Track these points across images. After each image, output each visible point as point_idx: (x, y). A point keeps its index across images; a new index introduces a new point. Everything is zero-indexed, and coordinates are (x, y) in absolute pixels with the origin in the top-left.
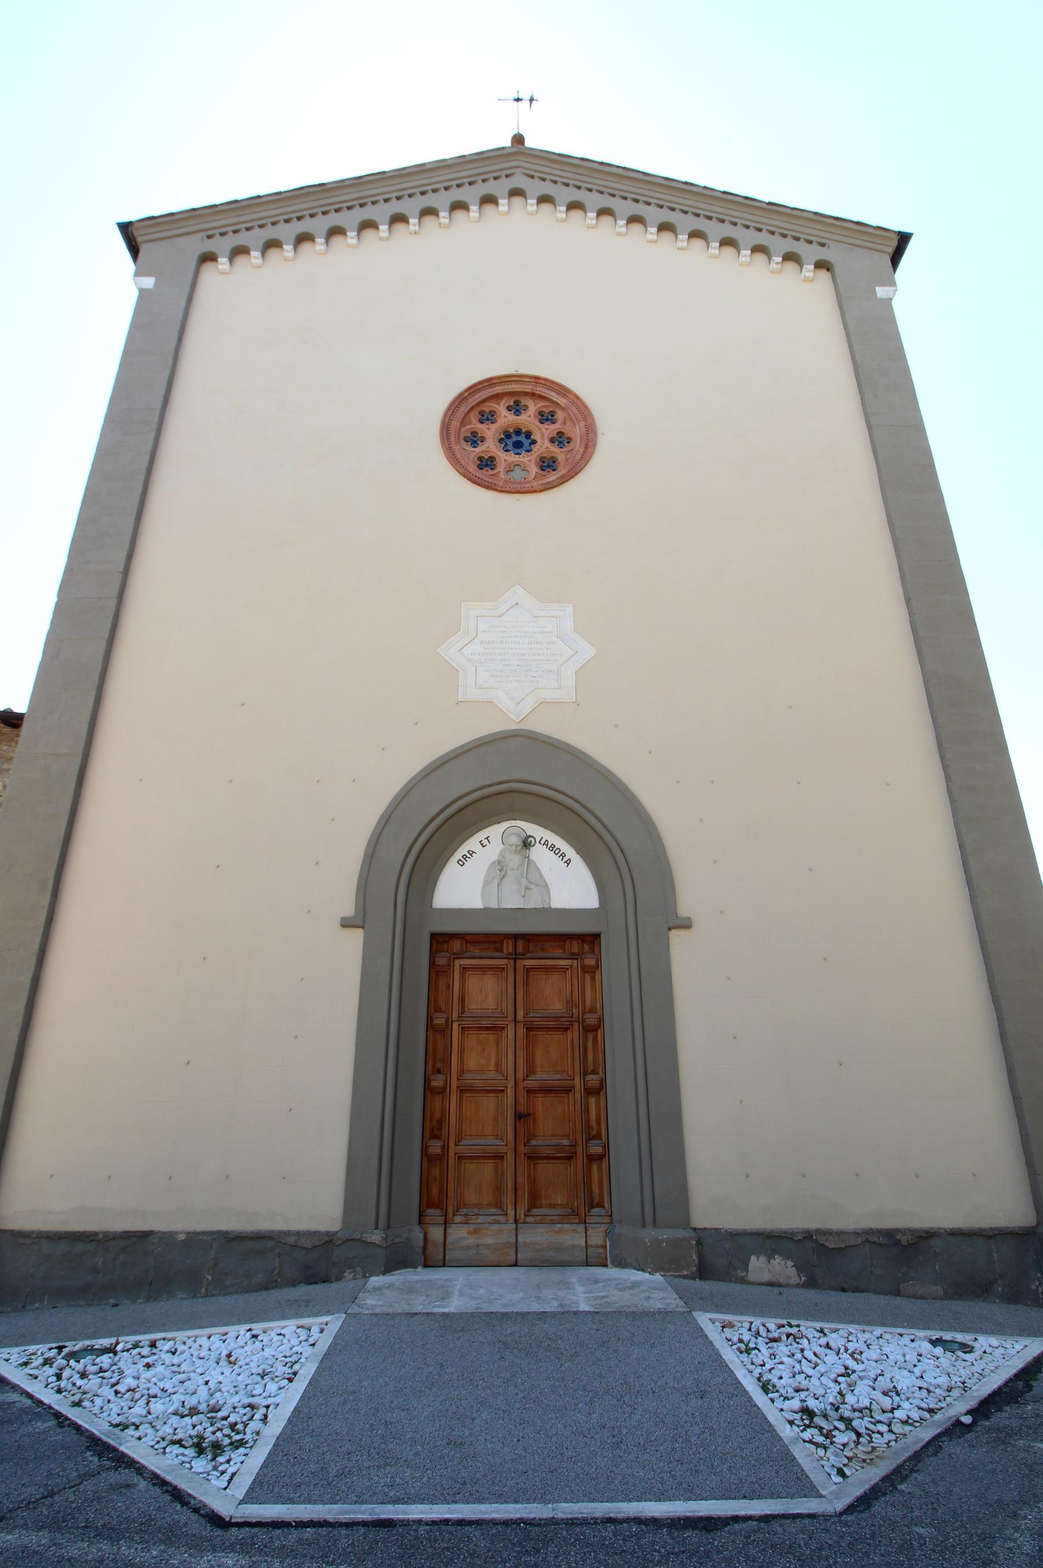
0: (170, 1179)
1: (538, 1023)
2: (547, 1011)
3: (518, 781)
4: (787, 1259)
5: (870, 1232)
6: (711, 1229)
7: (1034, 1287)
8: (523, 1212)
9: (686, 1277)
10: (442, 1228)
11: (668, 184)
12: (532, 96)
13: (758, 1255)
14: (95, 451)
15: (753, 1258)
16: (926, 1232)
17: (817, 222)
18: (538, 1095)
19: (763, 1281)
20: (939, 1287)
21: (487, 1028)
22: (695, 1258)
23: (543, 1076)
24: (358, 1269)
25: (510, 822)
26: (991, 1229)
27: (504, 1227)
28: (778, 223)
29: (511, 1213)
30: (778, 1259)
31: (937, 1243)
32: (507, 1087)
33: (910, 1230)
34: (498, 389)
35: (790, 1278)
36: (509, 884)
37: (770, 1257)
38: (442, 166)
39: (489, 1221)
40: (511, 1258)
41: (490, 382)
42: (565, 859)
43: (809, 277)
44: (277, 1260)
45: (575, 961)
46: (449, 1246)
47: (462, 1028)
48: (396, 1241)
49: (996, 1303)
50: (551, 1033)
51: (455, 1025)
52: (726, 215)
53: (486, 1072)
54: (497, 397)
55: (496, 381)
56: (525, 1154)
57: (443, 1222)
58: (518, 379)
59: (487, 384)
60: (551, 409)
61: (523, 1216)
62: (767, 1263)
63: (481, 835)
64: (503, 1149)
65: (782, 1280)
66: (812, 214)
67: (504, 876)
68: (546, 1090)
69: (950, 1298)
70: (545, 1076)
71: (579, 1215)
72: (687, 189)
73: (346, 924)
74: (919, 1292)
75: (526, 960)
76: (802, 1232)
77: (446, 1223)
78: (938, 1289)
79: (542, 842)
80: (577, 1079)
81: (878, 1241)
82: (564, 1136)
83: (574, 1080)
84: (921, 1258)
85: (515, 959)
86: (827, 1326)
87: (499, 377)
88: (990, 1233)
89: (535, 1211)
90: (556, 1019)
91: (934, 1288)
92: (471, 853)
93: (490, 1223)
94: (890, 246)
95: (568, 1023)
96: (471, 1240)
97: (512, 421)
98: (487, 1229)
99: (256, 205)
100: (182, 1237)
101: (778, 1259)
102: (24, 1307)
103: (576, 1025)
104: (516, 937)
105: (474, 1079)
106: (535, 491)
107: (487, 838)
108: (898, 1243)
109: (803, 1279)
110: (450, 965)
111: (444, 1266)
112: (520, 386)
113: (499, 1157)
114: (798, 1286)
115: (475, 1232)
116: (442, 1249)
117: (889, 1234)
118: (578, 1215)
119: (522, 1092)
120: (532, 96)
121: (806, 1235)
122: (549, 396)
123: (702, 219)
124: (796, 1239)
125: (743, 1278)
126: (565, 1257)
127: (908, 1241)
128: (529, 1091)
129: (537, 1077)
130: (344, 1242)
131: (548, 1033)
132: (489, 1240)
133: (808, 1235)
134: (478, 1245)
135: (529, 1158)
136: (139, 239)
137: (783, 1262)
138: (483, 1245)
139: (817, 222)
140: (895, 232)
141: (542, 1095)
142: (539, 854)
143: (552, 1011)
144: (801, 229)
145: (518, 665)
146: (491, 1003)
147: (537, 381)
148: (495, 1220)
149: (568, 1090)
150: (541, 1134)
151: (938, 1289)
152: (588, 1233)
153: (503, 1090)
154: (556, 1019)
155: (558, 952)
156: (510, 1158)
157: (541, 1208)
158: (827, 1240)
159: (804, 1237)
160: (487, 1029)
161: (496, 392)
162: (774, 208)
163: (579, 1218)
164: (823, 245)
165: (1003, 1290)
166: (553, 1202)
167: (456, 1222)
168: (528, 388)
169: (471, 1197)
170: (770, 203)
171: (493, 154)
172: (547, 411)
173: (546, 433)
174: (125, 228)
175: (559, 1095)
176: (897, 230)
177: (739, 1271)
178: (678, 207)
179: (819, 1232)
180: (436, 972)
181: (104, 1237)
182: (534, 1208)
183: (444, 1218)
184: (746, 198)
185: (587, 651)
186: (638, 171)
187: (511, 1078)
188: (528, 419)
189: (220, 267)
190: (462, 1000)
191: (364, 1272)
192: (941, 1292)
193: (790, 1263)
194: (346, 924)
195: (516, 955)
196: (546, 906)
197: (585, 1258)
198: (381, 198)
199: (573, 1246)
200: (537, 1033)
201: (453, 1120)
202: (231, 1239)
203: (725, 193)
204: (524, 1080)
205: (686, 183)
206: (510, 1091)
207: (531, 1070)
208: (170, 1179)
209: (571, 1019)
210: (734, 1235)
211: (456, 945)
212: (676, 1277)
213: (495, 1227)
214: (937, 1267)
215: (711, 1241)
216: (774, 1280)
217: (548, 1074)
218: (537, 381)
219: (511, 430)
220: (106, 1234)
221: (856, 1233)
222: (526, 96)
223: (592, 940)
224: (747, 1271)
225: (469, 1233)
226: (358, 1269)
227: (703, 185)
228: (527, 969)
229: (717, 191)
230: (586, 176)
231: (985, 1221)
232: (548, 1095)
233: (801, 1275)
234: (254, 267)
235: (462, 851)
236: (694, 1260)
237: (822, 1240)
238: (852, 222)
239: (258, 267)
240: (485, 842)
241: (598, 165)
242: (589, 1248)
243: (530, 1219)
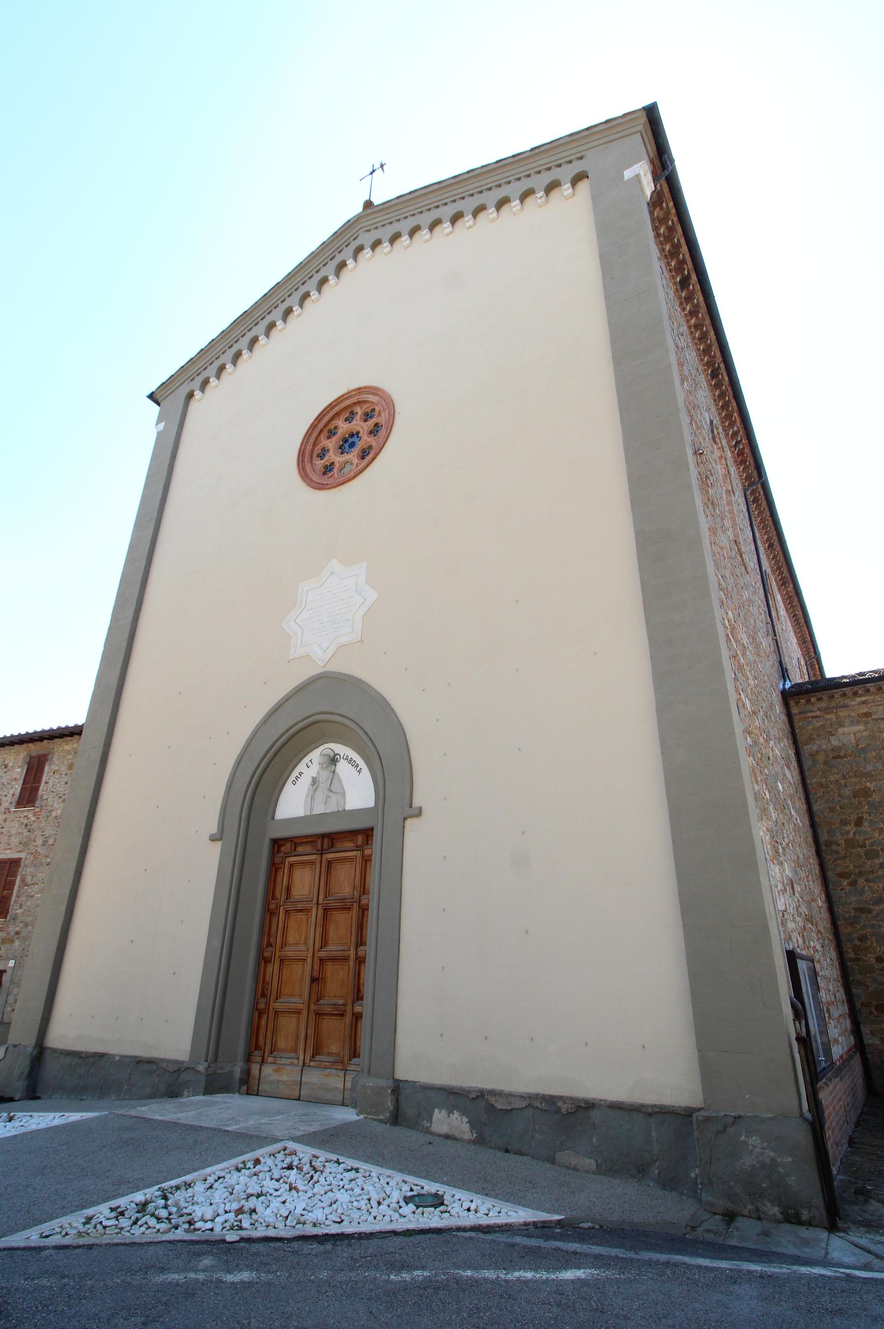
0: (442, 1036)
1: (331, 905)
2: (340, 895)
3: (320, 713)
4: (464, 1114)
5: (536, 1097)
6: (411, 1081)
7: (693, 1175)
8: (309, 1057)
9: (381, 1121)
10: (259, 1066)
11: (457, 181)
12: (381, 163)
13: (441, 1108)
14: (128, 548)
15: (437, 1111)
16: (586, 1101)
17: (573, 141)
18: (328, 963)
19: (442, 1133)
20: (592, 1161)
21: (301, 910)
22: (389, 1105)
23: (333, 948)
24: (191, 1090)
25: (324, 745)
26: (655, 1106)
27: (295, 1068)
28: (543, 161)
29: (301, 1057)
30: (456, 1114)
31: (596, 1115)
32: (307, 957)
33: (571, 1099)
34: (337, 409)
35: (464, 1133)
36: (320, 795)
37: (450, 1112)
38: (313, 256)
39: (287, 1062)
40: (296, 1093)
41: (331, 406)
42: (358, 769)
43: (569, 194)
44: (157, 1079)
45: (359, 852)
46: (262, 1080)
47: (286, 911)
48: (219, 1071)
49: (649, 1186)
50: (341, 912)
51: (282, 908)
52: (437, 202)
53: (298, 945)
54: (337, 415)
55: (335, 404)
56: (314, 1011)
57: (261, 1061)
58: (348, 395)
59: (329, 409)
60: (372, 408)
61: (308, 1060)
62: (447, 1116)
63: (306, 760)
64: (301, 1006)
65: (457, 1134)
66: (567, 137)
67: (316, 789)
68: (333, 959)
69: (604, 1174)
70: (334, 948)
71: (341, 1064)
72: (472, 175)
73: (213, 839)
74: (573, 1163)
75: (328, 855)
76: (476, 1091)
77: (263, 1062)
78: (591, 1163)
79: (345, 758)
80: (352, 950)
81: (540, 1107)
82: (342, 997)
83: (350, 950)
84: (579, 1128)
85: (322, 854)
86: (363, 1167)
87: (336, 400)
88: (650, 1110)
89: (318, 1058)
90: (342, 901)
91: (588, 1161)
92: (301, 774)
93: (288, 1065)
94: (640, 124)
95: (350, 904)
96: (275, 1077)
97: (346, 428)
98: (284, 1069)
99: (214, 345)
100: (117, 1058)
101: (456, 1114)
102: (51, 1096)
103: (355, 905)
104: (323, 836)
105: (289, 951)
106: (349, 480)
107: (311, 761)
108: (558, 1111)
109: (475, 1135)
110: (283, 862)
111: (257, 1095)
112: (348, 401)
113: (298, 1012)
114: (470, 1141)
115: (277, 1071)
116: (257, 1082)
117: (551, 1099)
118: (342, 1063)
119: (317, 961)
120: (381, 163)
121: (479, 1094)
122: (367, 399)
123: (575, 163)
124: (471, 1097)
125: (428, 1128)
126: (329, 1096)
127: (568, 1109)
128: (322, 960)
129: (330, 948)
130: (185, 1070)
131: (340, 912)
132: (285, 1078)
133: (482, 1094)
134: (278, 1081)
135: (316, 1014)
136: (159, 401)
137: (460, 1118)
138: (281, 1081)
139: (573, 141)
140: (640, 110)
141: (331, 963)
142: (343, 767)
143: (343, 894)
144: (567, 153)
145: (328, 622)
146: (306, 891)
147: (360, 391)
148: (292, 1062)
149: (346, 959)
150: (328, 995)
151: (591, 1163)
152: (346, 1078)
153: (305, 959)
154: (342, 901)
155: (350, 845)
156: (305, 1013)
157: (322, 1055)
158: (496, 1100)
159: (477, 1097)
160: (301, 911)
161: (335, 412)
162: (537, 151)
163: (343, 1065)
164: (581, 158)
165: (659, 1173)
166: (331, 1051)
167: (269, 1061)
168: (354, 400)
169: (282, 1043)
170: (532, 150)
171: (343, 229)
172: (369, 411)
173: (366, 428)
174: (151, 397)
175: (342, 963)
176: (640, 107)
177: (425, 1121)
178: (532, 172)
179: (492, 1093)
180: (274, 867)
181: (85, 1055)
182: (319, 1055)
183: (261, 1058)
184: (514, 156)
185: (372, 595)
186: (434, 184)
187: (311, 950)
188: (343, 427)
189: (196, 397)
190: (289, 889)
191: (194, 1092)
192: (593, 1167)
193: (465, 1119)
194: (213, 839)
195: (322, 850)
196: (340, 809)
197: (342, 1098)
198: (279, 302)
199: (336, 1088)
200: (333, 912)
201: (275, 983)
202: (139, 1061)
203: (497, 162)
204: (319, 951)
205: (468, 172)
206: (309, 960)
207: (324, 943)
208: (442, 1036)
209: (352, 900)
210: (427, 1088)
211: (288, 847)
212: (374, 1120)
213: (289, 1068)
214: (594, 1140)
215: (408, 1091)
216: (450, 1133)
217: (336, 946)
218: (360, 391)
219: (347, 436)
220: (87, 1053)
221: (522, 1097)
222: (377, 166)
223: (367, 833)
224: (431, 1123)
225: (275, 1071)
226: (191, 1090)
227: (529, 149)
228: (329, 861)
229: (492, 164)
230: (403, 208)
231: (650, 1098)
232: (335, 963)
233: (473, 1132)
234: (214, 388)
235: (295, 773)
236: (389, 1107)
237: (492, 1100)
238: (601, 124)
239: (216, 387)
240: (310, 764)
241: (409, 195)
242: (346, 1091)
243: (312, 1064)
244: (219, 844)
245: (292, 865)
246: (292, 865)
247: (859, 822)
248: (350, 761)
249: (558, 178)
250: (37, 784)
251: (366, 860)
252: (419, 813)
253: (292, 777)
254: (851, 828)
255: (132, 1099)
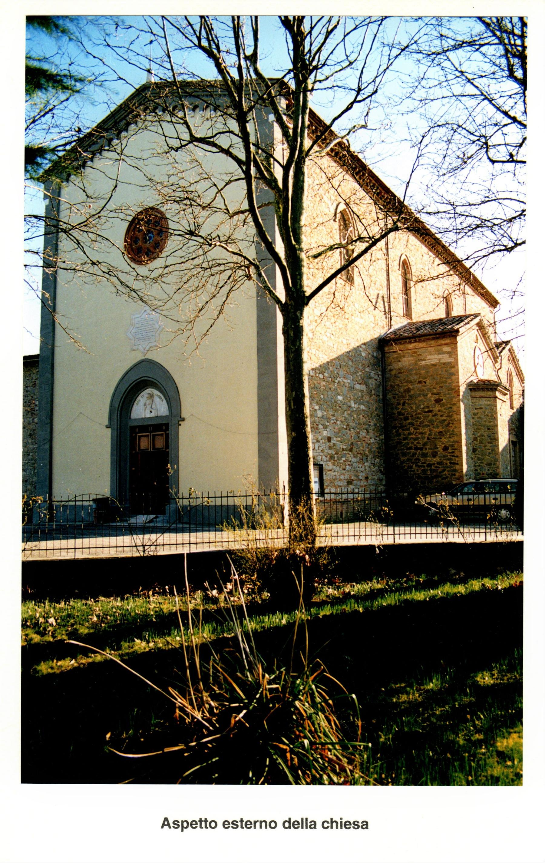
63: (142, 394)
194: (107, 427)
223: (167, 425)
235: (137, 400)
244: (110, 430)
245: (140, 437)
246: (140, 437)
247: (404, 404)
248: (159, 397)
249: (138, 357)
250: (291, 778)
251: (167, 436)
252: (183, 420)
253: (136, 402)
254: (400, 407)
255: (89, 529)
